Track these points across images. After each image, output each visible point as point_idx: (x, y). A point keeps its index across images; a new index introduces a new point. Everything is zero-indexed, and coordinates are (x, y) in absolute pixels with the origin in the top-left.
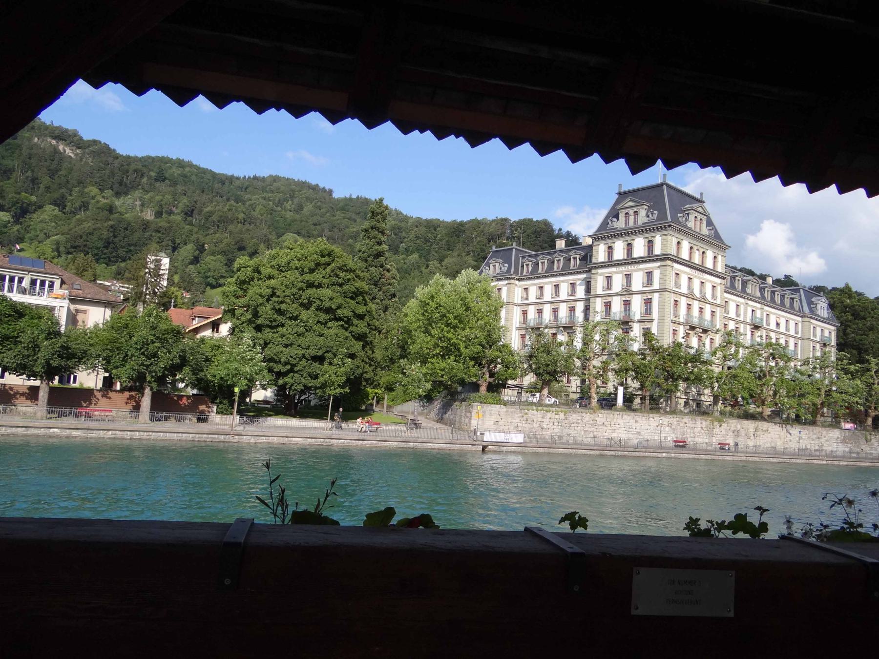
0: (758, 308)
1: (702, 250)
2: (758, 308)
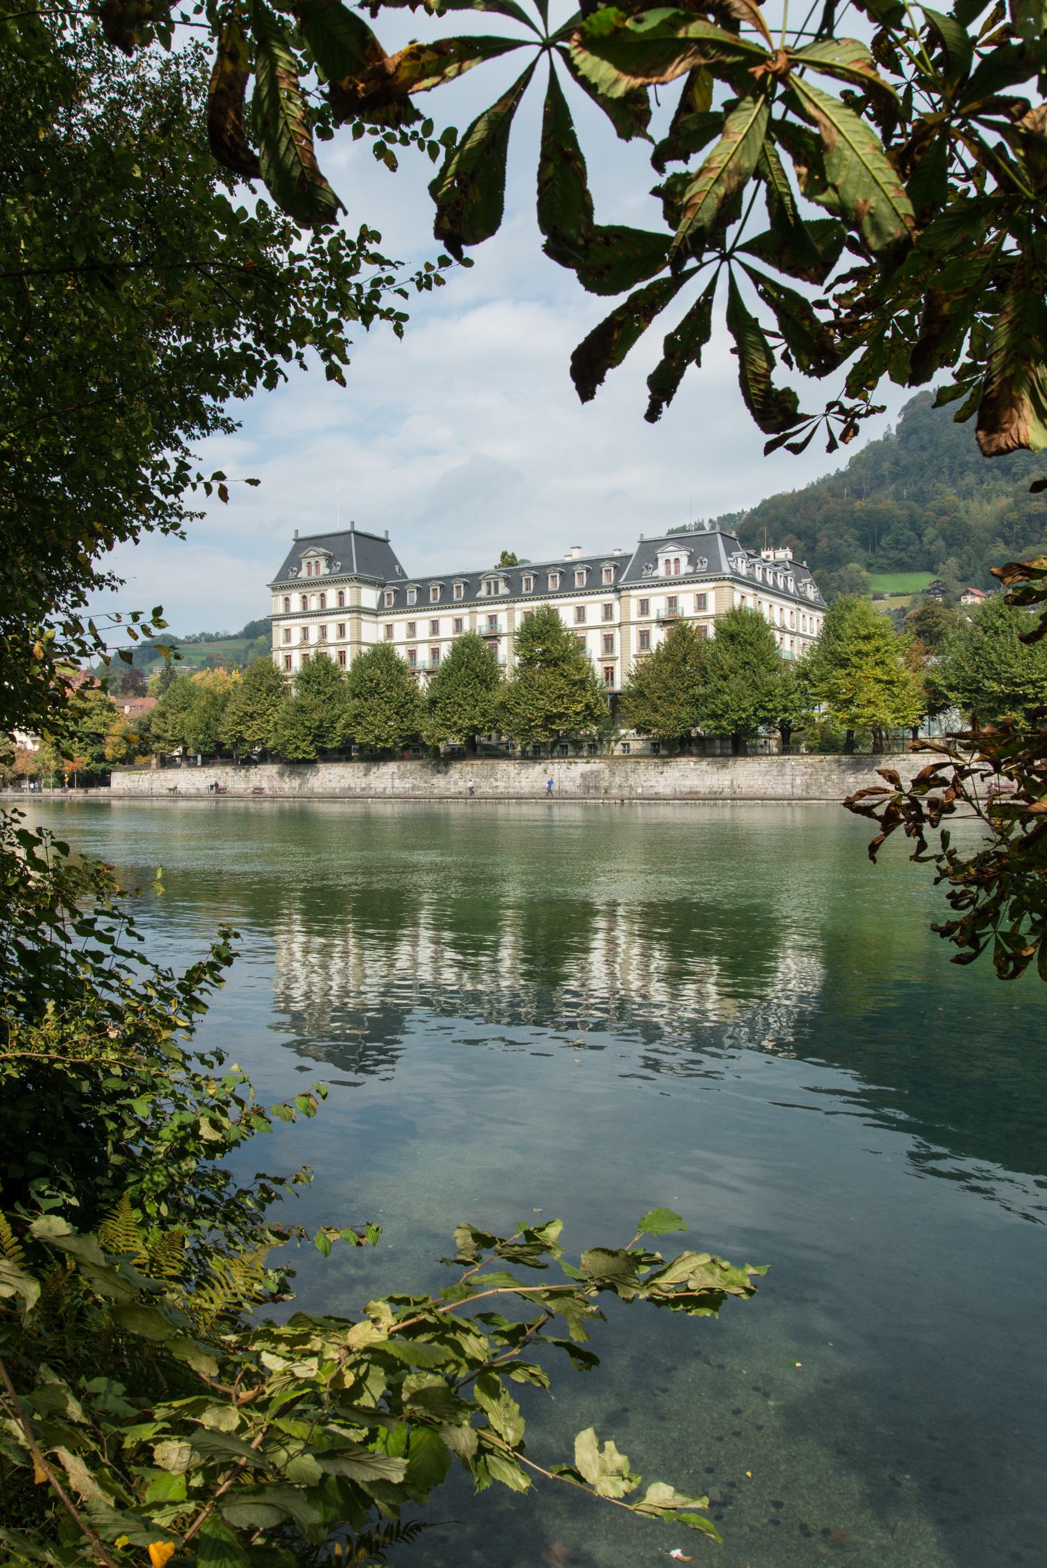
0: (501, 611)
1: (318, 594)
2: (501, 611)
